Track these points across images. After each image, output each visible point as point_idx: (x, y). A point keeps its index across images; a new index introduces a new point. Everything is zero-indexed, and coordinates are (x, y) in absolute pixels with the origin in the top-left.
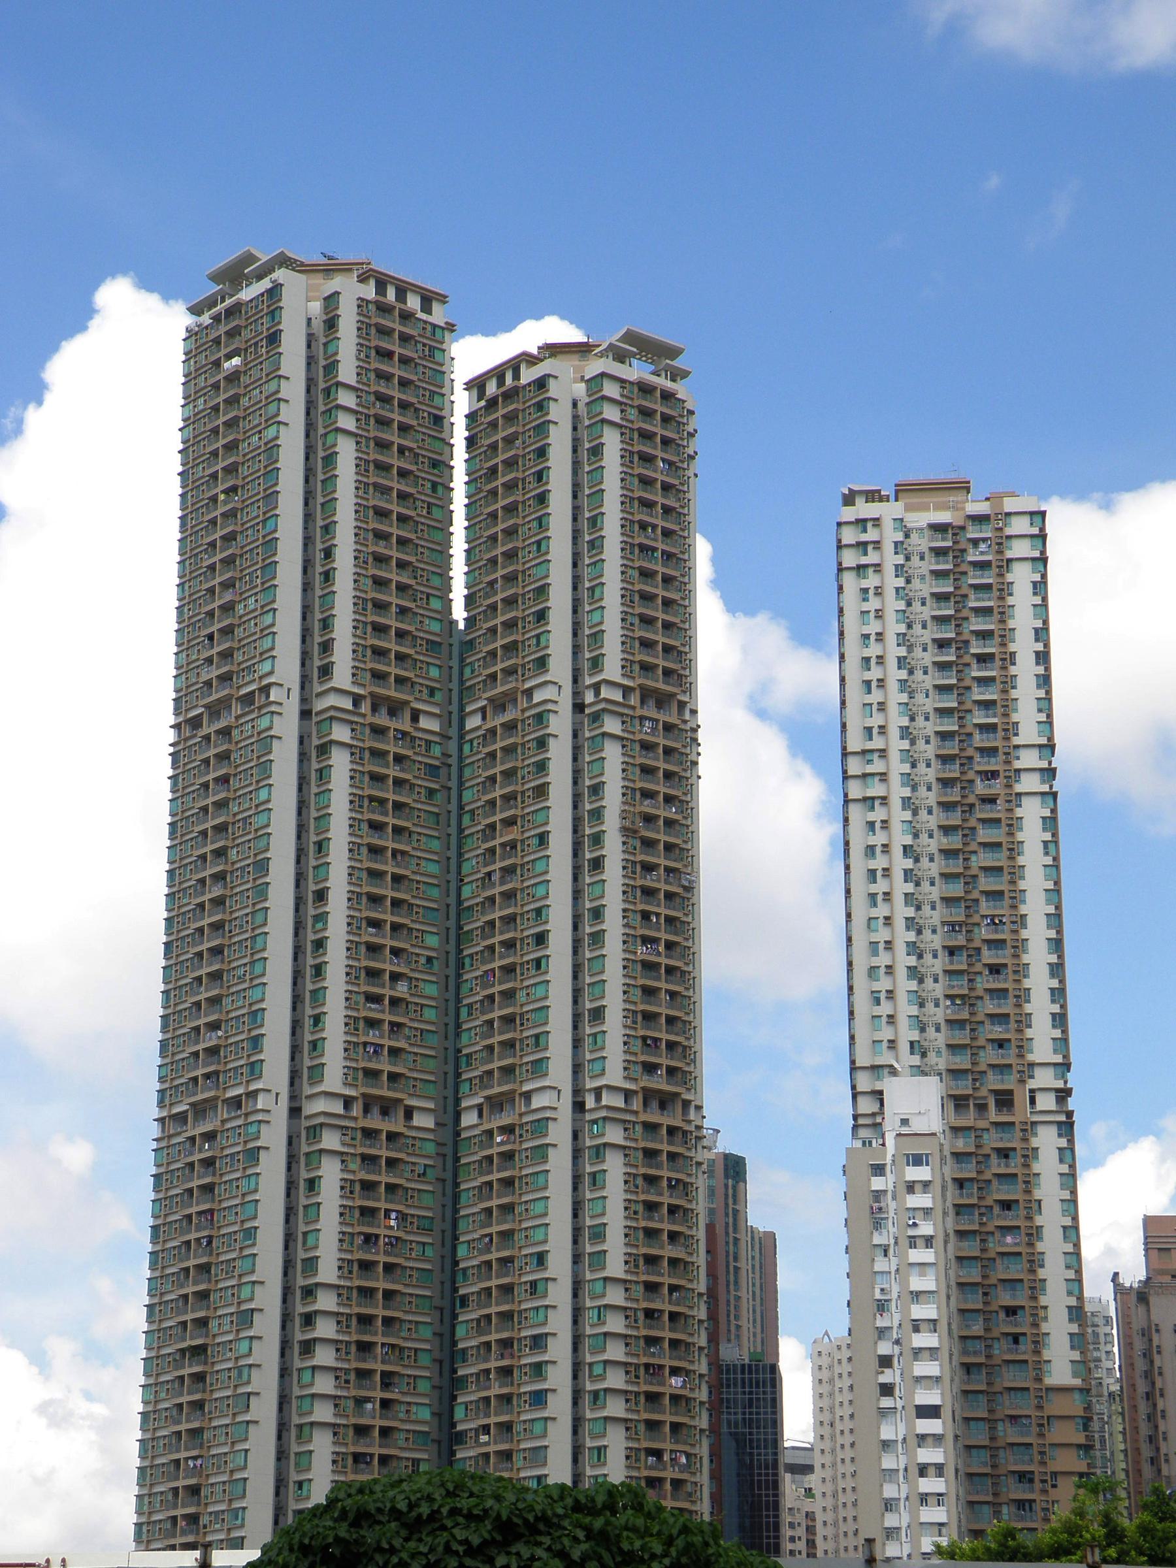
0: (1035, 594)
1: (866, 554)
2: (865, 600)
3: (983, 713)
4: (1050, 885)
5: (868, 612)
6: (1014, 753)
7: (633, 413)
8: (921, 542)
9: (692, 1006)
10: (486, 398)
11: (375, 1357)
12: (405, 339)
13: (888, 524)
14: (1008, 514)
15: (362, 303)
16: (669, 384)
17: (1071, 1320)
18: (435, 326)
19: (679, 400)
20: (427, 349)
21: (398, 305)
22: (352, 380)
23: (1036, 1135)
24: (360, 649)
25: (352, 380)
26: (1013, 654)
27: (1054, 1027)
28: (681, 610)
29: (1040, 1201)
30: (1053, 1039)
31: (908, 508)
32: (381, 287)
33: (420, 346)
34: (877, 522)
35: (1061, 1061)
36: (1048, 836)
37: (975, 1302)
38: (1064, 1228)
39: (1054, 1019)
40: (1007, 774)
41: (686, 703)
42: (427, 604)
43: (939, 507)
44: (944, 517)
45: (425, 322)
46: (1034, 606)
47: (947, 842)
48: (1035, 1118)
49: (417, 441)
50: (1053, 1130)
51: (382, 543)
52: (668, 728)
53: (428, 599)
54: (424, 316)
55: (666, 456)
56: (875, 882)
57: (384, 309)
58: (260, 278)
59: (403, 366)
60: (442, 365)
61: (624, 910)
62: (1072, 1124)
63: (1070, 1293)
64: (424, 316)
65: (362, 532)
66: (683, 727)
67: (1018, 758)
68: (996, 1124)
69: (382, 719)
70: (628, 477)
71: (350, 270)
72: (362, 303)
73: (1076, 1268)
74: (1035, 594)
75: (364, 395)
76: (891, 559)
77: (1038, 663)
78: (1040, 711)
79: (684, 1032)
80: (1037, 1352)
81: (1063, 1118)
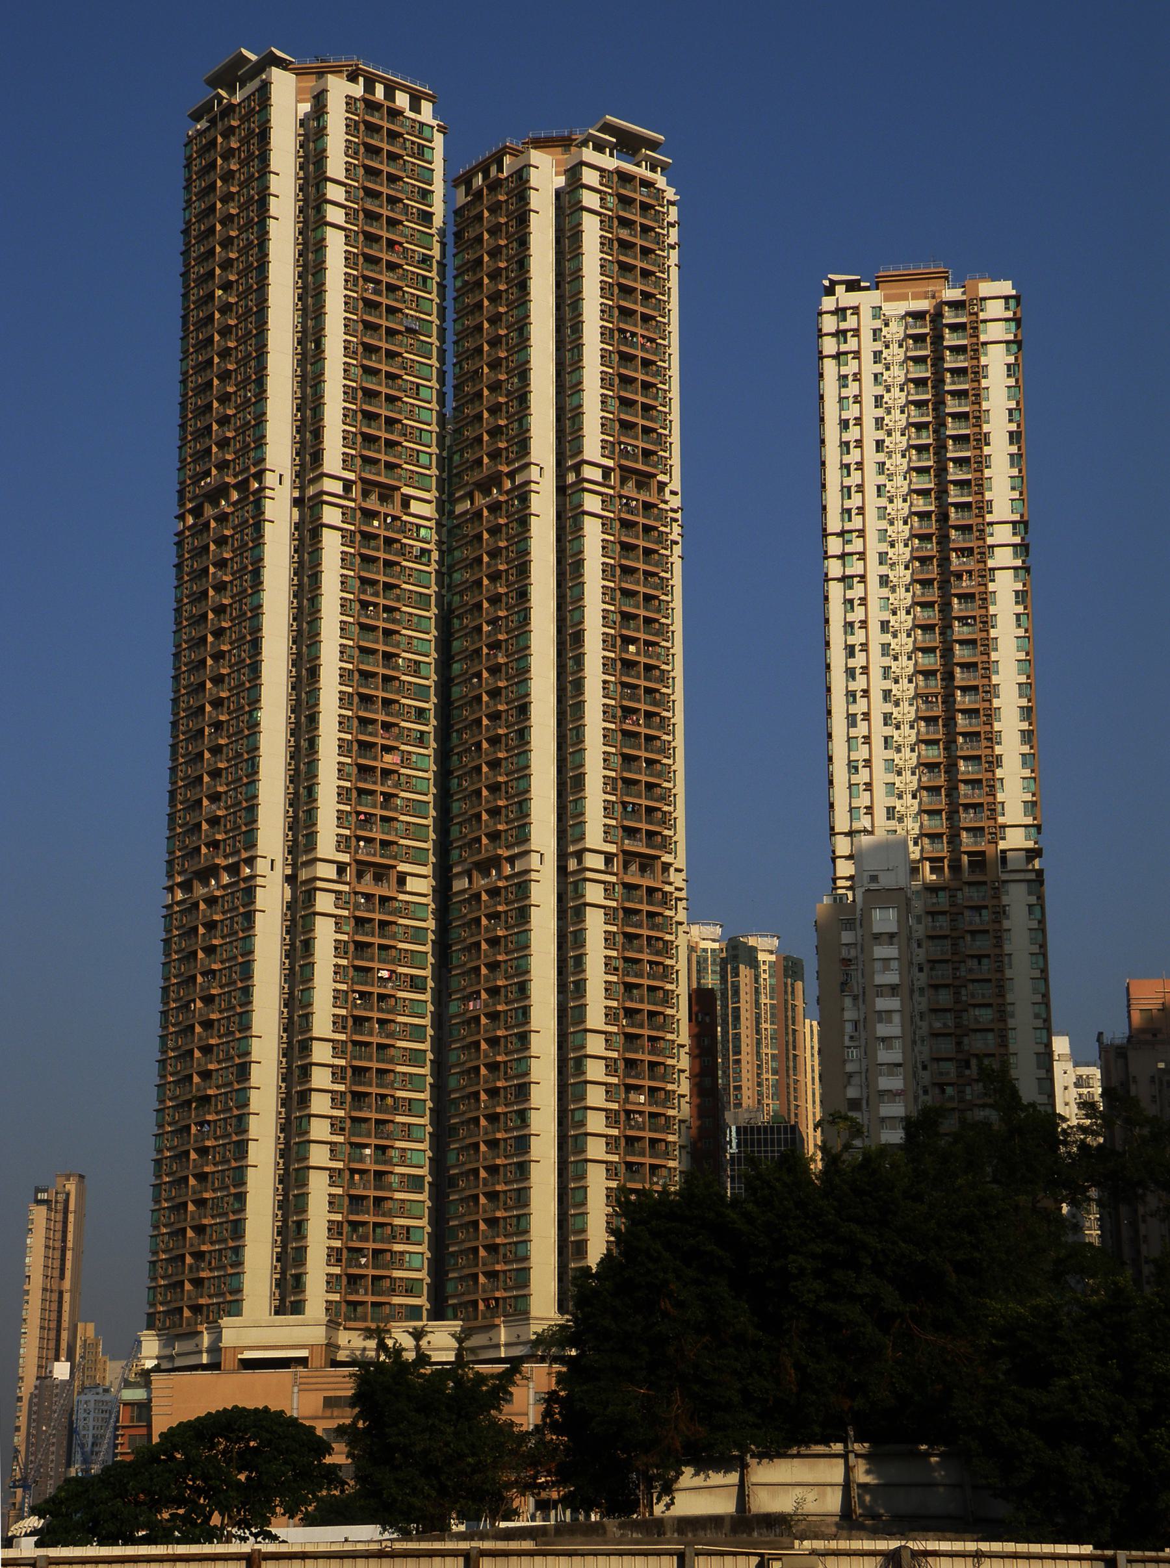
0: (1009, 376)
1: (845, 320)
2: (846, 386)
3: (952, 314)
4: (1038, 998)
5: (847, 398)
6: (988, 530)
7: (612, 201)
8: (895, 331)
9: (672, 775)
10: (472, 192)
11: (370, 1107)
12: (393, 136)
13: (866, 313)
14: (984, 299)
15: (350, 101)
16: (649, 174)
17: (1017, 603)
18: (422, 124)
19: (659, 190)
20: (416, 147)
21: (386, 103)
22: (341, 175)
23: (1007, 893)
24: (351, 436)
25: (341, 175)
26: (987, 435)
27: (1017, 603)
28: (662, 417)
29: (1002, 779)
30: (1037, 1054)
31: (887, 299)
32: (369, 88)
33: (408, 144)
34: (856, 310)
35: (1043, 1051)
36: (1033, 900)
37: (947, 1047)
38: (1030, 906)
39: (1017, 596)
40: (982, 550)
41: (666, 484)
42: (418, 394)
43: (916, 297)
44: (923, 305)
45: (414, 121)
46: (1008, 387)
47: (916, 416)
48: (1005, 877)
49: (406, 236)
50: (1023, 887)
51: (370, 590)
52: (648, 506)
53: (408, 1232)
54: (412, 115)
55: (646, 333)
56: (853, 634)
57: (372, 106)
58: (252, 79)
59: (391, 163)
60: (431, 163)
61: (605, 682)
62: (1042, 883)
63: (1037, 1016)
64: (412, 115)
65: (348, 557)
66: (662, 506)
67: (992, 535)
68: (970, 884)
69: (373, 503)
70: (607, 264)
71: (341, 71)
72: (350, 101)
73: (1044, 1016)
74: (1009, 376)
75: (352, 190)
76: (868, 346)
77: (1011, 443)
78: (1013, 489)
79: (663, 634)
80: (1000, 970)
81: (1032, 876)
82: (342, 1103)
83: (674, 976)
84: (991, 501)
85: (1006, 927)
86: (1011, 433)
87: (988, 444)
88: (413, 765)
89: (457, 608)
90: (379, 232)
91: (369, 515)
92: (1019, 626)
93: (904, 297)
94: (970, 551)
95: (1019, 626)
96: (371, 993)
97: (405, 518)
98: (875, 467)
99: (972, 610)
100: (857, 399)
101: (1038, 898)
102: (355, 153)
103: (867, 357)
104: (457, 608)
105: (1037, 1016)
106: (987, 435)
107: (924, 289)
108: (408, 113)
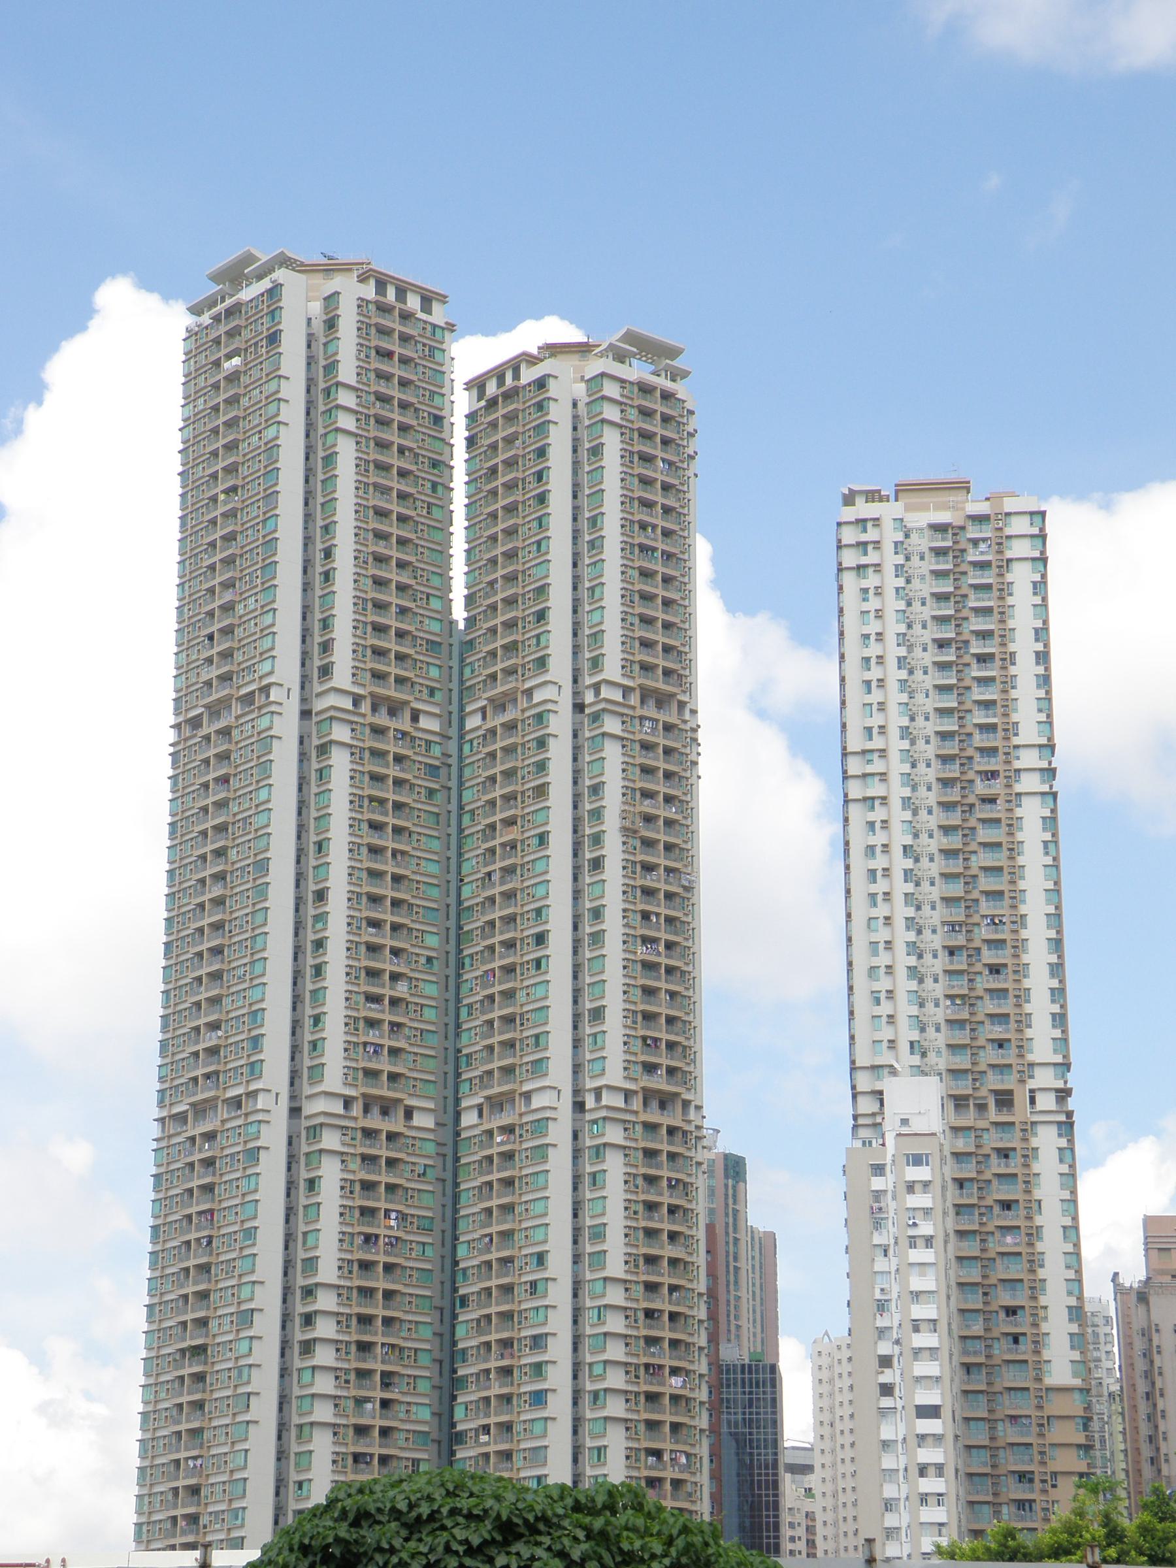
3: (983, 713)
5: (868, 612)
6: (1014, 753)
10: (486, 398)
11: (375, 1357)
12: (405, 339)
13: (888, 525)
14: (1008, 514)
15: (362, 303)
18: (434, 326)
20: (427, 349)
21: (398, 305)
22: (352, 380)
23: (1036, 1135)
25: (352, 380)
29: (1040, 1201)
31: (908, 508)
33: (420, 346)
34: (876, 521)
37: (975, 1301)
39: (1054, 1020)
43: (939, 507)
45: (425, 322)
48: (1035, 1118)
49: (417, 441)
50: (1054, 1130)
51: (382, 543)
53: (428, 599)
56: (875, 882)
57: (384, 309)
58: (260, 277)
60: (442, 387)
63: (1070, 1293)
67: (1018, 758)
68: (996, 1124)
69: (382, 719)
71: (350, 270)
72: (362, 303)
74: (1035, 594)
76: (891, 559)
77: (1038, 663)
78: (1040, 711)
81: (1063, 1118)
82: (347, 1353)
83: (698, 1465)
84: (1029, 989)
85: (1034, 1146)
86: (1054, 1015)
87: (1014, 664)
88: (427, 628)
89: (467, 899)
90: (390, 461)
91: (378, 731)
92: (1047, 854)
93: (925, 508)
94: (986, 611)
95: (1047, 854)
96: (391, 489)
97: (415, 734)
98: (896, 685)
99: (997, 859)
100: (879, 614)
101: (1053, 835)
102: (367, 356)
103: (889, 570)
104: (467, 899)
105: (1070, 1293)
106: (1039, 1228)
107: (944, 499)
108: (421, 315)
